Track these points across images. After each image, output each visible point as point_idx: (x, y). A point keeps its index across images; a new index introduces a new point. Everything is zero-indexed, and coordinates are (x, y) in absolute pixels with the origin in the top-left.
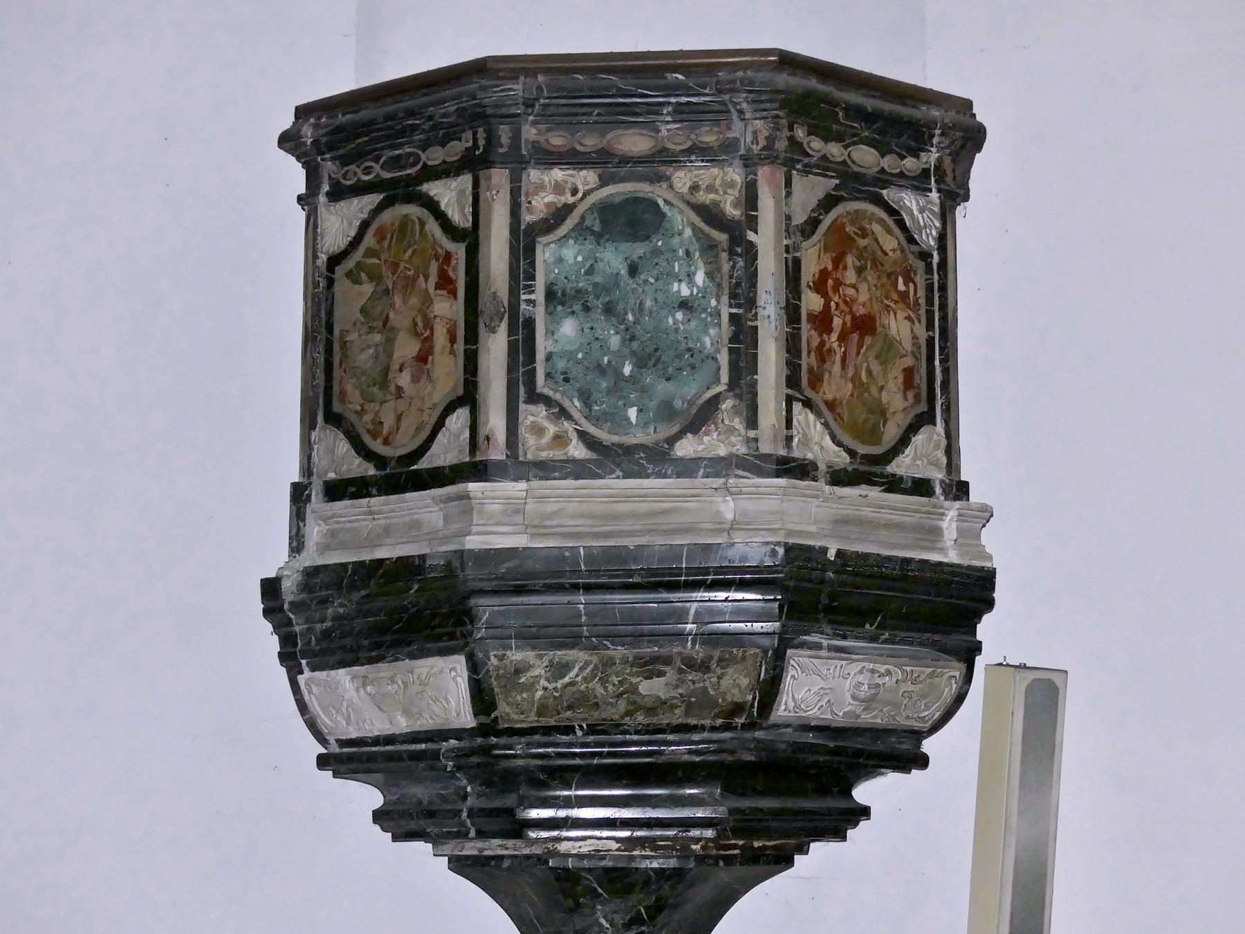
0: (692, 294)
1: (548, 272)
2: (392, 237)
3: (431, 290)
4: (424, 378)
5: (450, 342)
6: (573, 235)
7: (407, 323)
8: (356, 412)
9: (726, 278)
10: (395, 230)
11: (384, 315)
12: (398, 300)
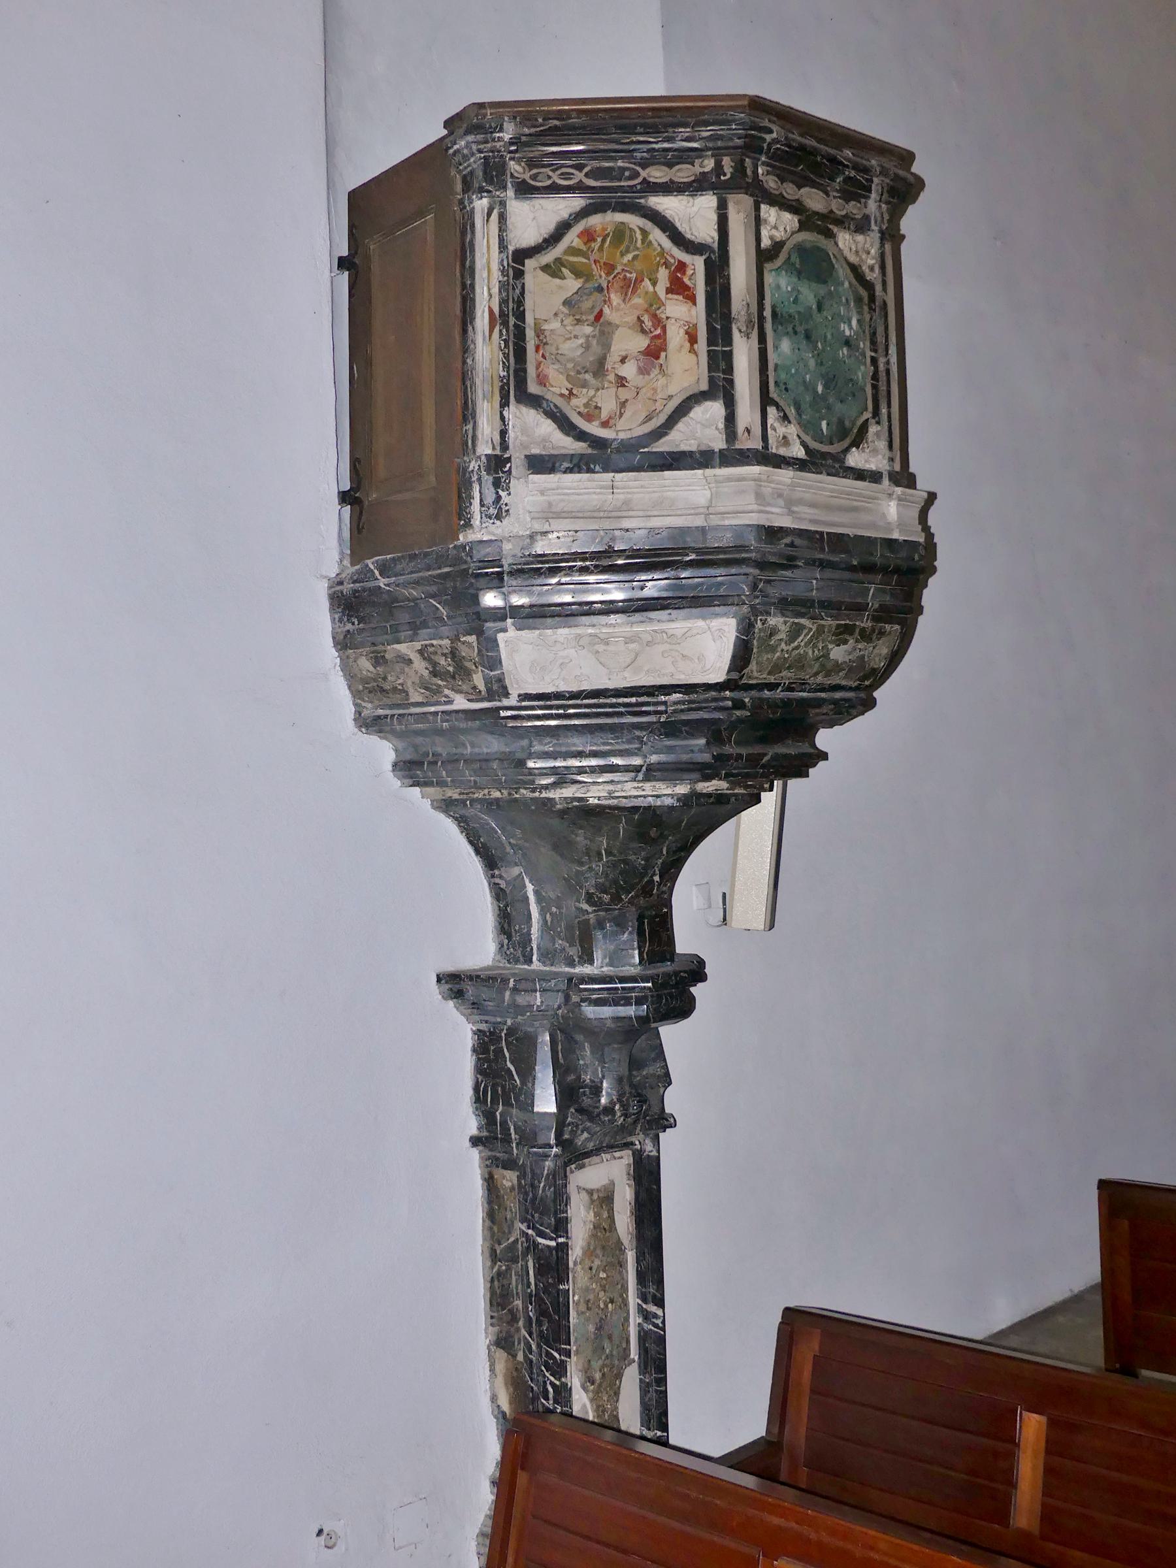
0: (850, 335)
1: (773, 295)
2: (604, 241)
3: (661, 293)
4: (656, 371)
5: (689, 341)
6: (785, 267)
7: (631, 318)
8: (562, 395)
9: (867, 327)
10: (608, 235)
11: (596, 311)
12: (615, 299)
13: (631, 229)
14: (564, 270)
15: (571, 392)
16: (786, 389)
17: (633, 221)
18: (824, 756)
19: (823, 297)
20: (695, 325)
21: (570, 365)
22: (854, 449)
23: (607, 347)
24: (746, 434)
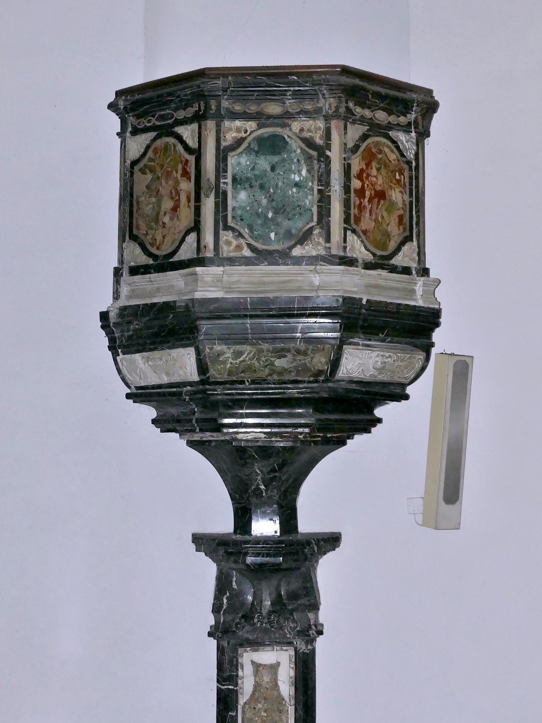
2: (160, 153)
8: (144, 234)
11: (157, 189)
13: (170, 145)
14: (147, 169)
15: (147, 233)
16: (242, 220)
17: (171, 140)
18: (379, 421)
19: (276, 163)
20: (190, 193)
21: (147, 219)
22: (299, 246)
23: (160, 207)
24: (204, 249)
